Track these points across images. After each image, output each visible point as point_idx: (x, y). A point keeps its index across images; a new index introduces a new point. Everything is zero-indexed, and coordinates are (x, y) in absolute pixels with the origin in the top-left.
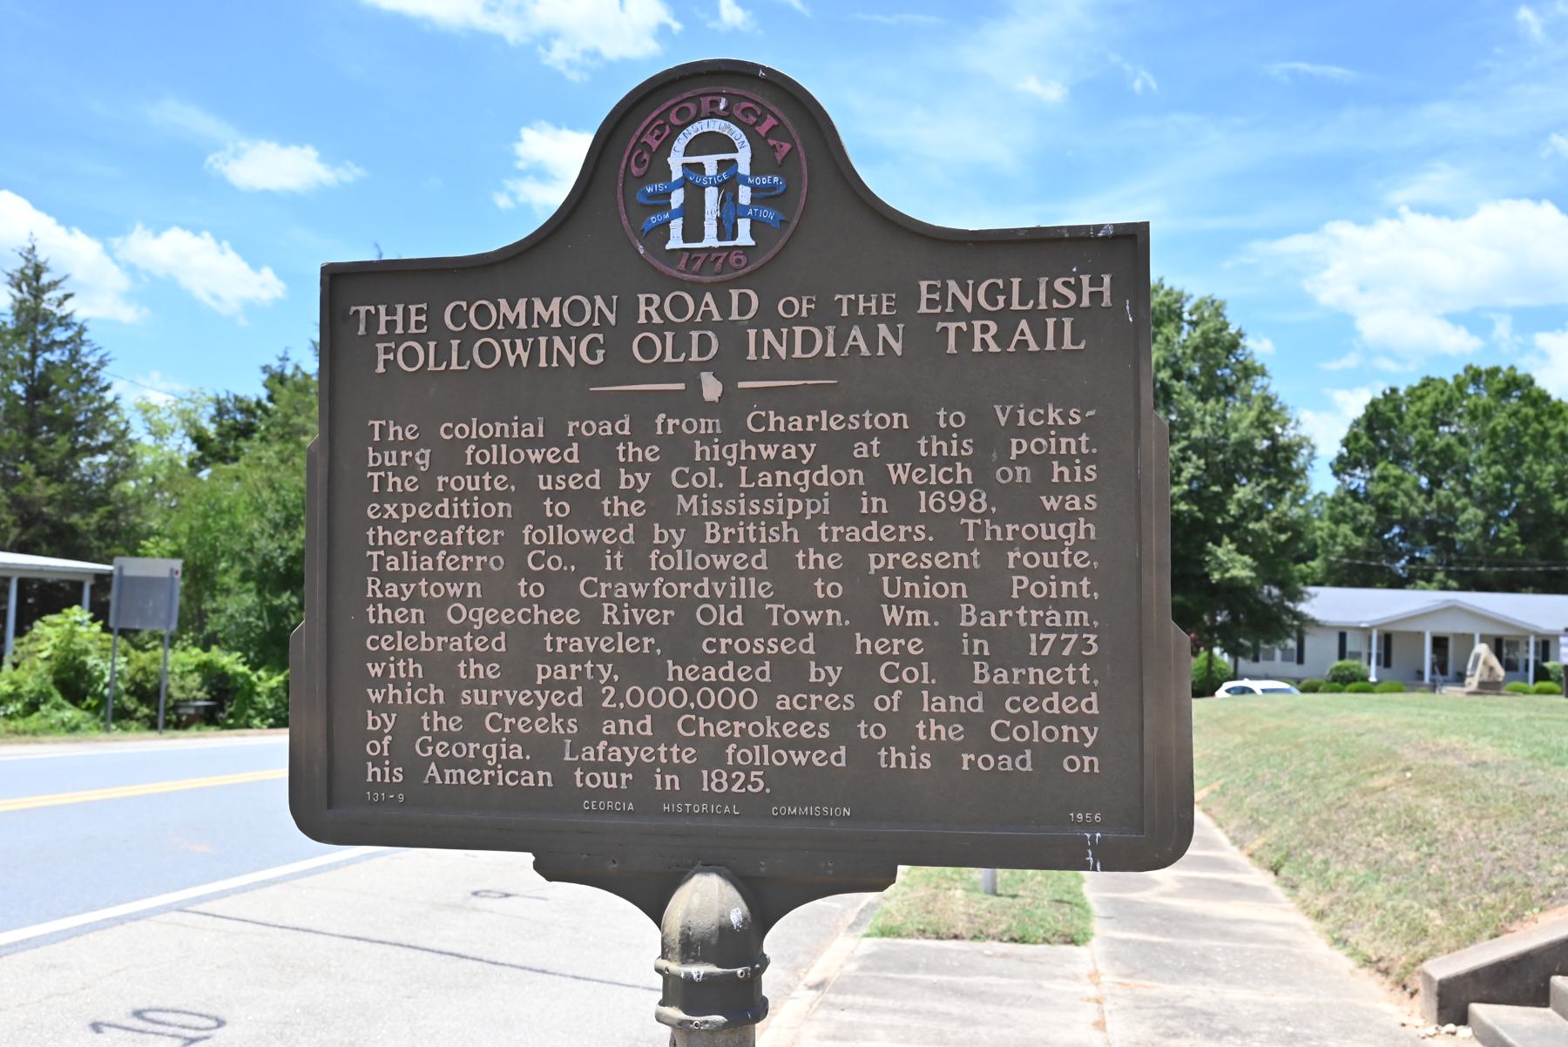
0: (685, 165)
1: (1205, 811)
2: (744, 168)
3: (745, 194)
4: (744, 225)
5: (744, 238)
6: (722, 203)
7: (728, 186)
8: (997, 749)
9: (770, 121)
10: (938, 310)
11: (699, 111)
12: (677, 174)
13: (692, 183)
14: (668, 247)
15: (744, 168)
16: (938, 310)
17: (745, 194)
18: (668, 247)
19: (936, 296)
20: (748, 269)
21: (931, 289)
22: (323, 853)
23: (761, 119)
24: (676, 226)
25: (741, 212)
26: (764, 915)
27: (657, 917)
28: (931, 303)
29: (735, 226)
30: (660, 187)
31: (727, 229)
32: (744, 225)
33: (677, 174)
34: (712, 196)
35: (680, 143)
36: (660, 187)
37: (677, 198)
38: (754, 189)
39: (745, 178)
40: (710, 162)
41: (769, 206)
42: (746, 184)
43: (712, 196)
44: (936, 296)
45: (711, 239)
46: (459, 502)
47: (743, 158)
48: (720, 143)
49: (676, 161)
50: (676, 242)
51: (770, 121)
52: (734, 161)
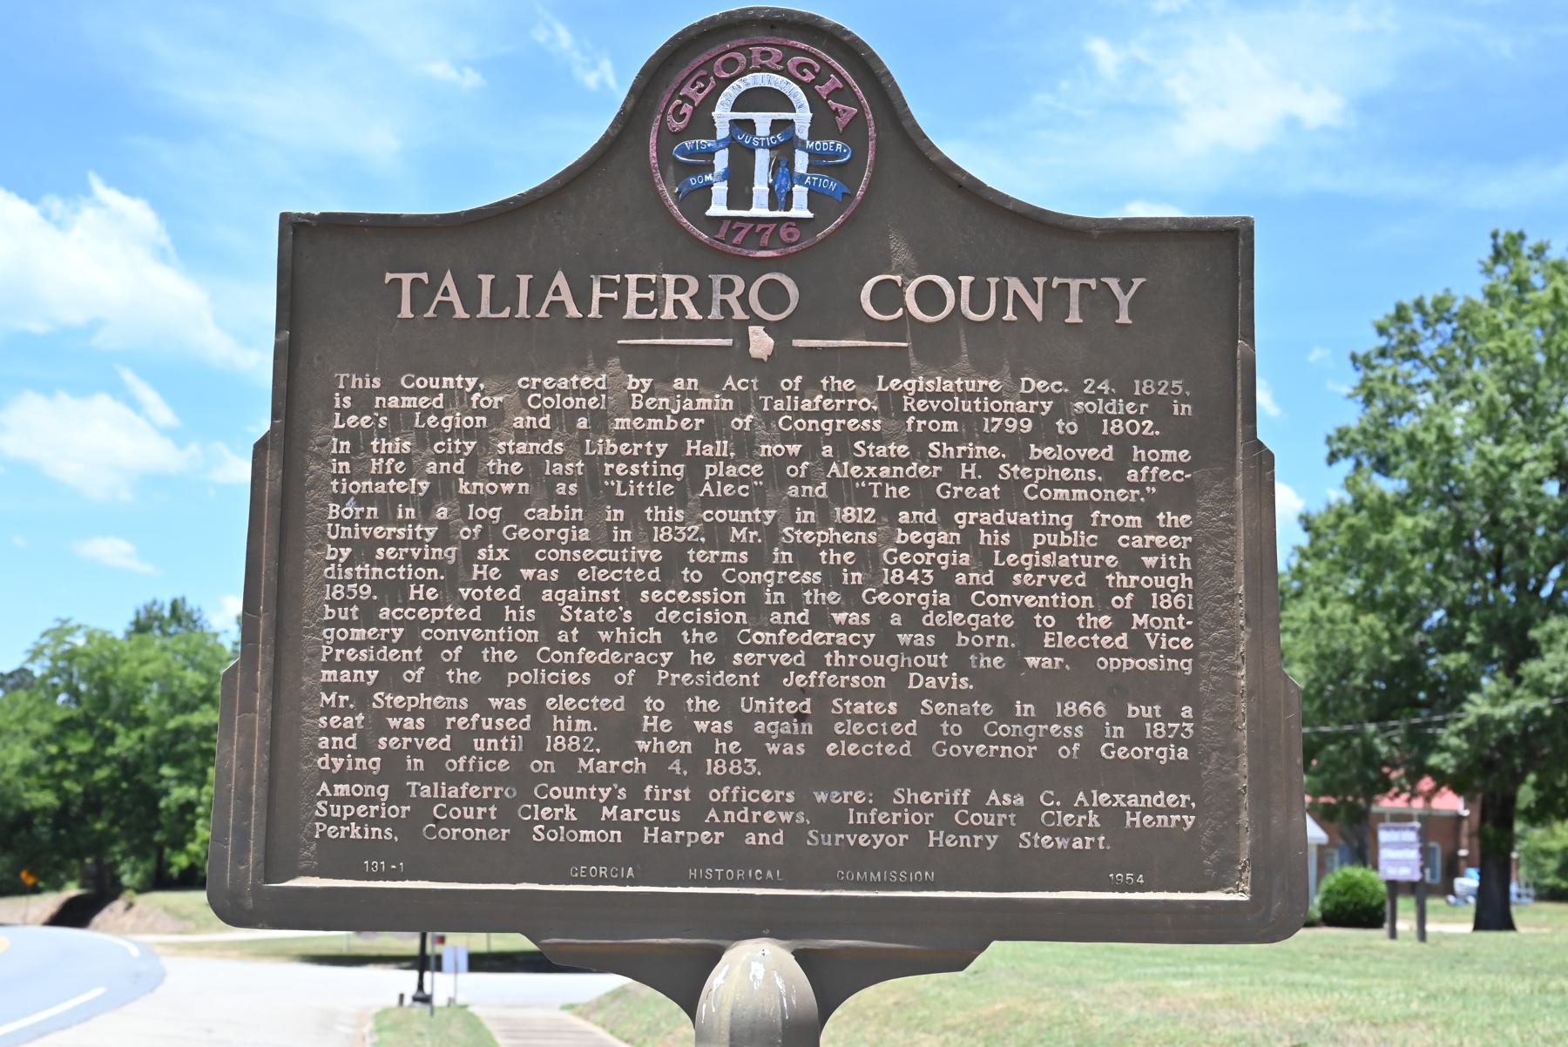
0: (734, 123)
1: (617, 995)
2: (802, 132)
3: (801, 161)
4: (800, 193)
5: (800, 209)
6: (774, 169)
7: (785, 144)
8: (959, 831)
9: (833, 82)
10: (652, 316)
11: (749, 63)
12: (723, 132)
13: (741, 145)
14: (708, 213)
15: (802, 132)
16: (652, 316)
17: (801, 161)
18: (708, 213)
19: (651, 296)
20: (803, 245)
21: (643, 286)
22: (220, 930)
23: (820, 79)
24: (720, 190)
25: (793, 178)
26: (827, 1005)
27: (690, 1008)
28: (642, 305)
29: (790, 194)
30: (710, 144)
31: (780, 198)
32: (800, 193)
33: (723, 132)
34: (762, 158)
35: (731, 93)
36: (710, 144)
37: (721, 160)
38: (812, 154)
39: (804, 142)
40: (763, 121)
41: (832, 176)
42: (803, 149)
43: (762, 158)
44: (651, 296)
45: (760, 209)
46: (635, 484)
47: (802, 117)
48: (779, 101)
49: (723, 114)
50: (718, 209)
51: (833, 82)
52: (791, 122)
